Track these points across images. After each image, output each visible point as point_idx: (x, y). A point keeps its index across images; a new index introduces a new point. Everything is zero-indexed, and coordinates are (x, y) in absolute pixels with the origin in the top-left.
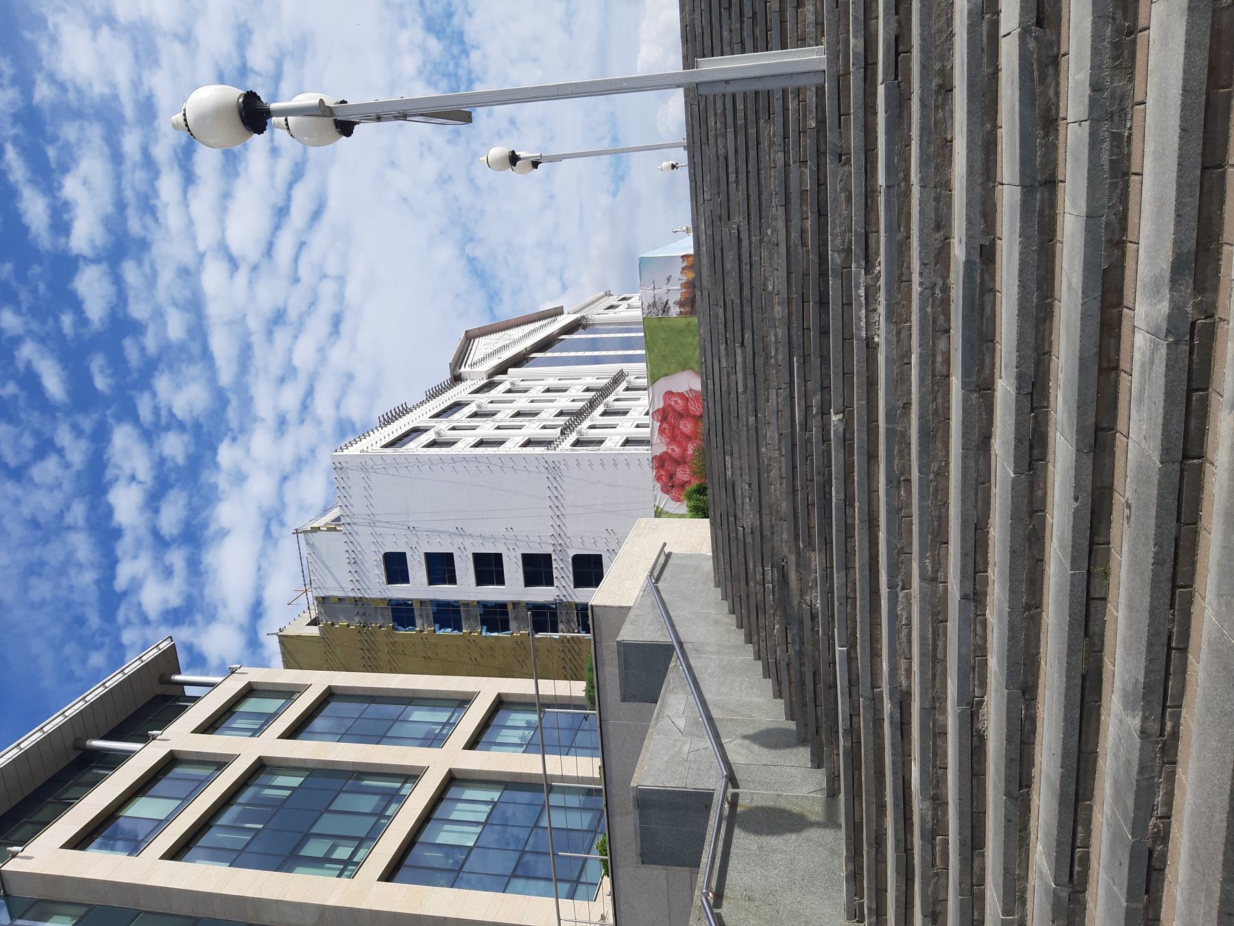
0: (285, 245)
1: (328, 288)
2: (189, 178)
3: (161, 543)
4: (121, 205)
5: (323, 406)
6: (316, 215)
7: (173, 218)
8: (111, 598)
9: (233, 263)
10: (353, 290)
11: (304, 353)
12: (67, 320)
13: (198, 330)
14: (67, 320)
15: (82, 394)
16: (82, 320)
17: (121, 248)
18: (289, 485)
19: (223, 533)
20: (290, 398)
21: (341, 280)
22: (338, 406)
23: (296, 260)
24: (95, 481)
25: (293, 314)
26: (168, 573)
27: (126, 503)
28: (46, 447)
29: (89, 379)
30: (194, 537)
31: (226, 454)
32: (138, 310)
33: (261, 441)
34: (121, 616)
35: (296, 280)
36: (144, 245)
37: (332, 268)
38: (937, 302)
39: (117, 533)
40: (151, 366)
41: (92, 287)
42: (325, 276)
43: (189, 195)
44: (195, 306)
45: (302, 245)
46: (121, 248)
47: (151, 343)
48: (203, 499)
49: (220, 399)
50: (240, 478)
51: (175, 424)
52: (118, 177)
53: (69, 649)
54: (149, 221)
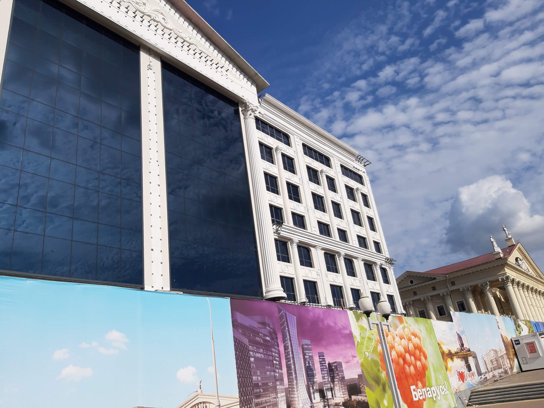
0: (510, 92)
1: (498, 114)
2: (532, 44)
3: (373, 92)
4: (511, 24)
5: (441, 130)
6: (532, 97)
7: (513, 44)
8: (349, 83)
9: (497, 74)
10: (499, 124)
11: (463, 115)
12: (457, 23)
13: (464, 70)
14: (457, 23)
15: (426, 42)
16: (457, 28)
17: (492, 30)
18: (404, 129)
19: (380, 111)
20: (441, 117)
21: (504, 117)
22: (443, 136)
23: (506, 97)
24: (394, 58)
25: (482, 105)
26: (362, 98)
27: (388, 72)
28: (404, 37)
29: (432, 43)
30: (378, 103)
31: (413, 101)
32: (467, 46)
33: (421, 112)
34: (344, 88)
35: (497, 100)
36: (496, 37)
37: (508, 112)
38: (189, 103)
39: (376, 76)
40: (444, 60)
41: (475, 25)
42: (503, 110)
43: (523, 47)
44: (475, 65)
45: (514, 98)
46: (492, 30)
47: (454, 56)
48: (394, 99)
49: (436, 90)
50: (404, 110)
51: (422, 76)
52: (525, 17)
53: (329, 76)
54: (508, 36)
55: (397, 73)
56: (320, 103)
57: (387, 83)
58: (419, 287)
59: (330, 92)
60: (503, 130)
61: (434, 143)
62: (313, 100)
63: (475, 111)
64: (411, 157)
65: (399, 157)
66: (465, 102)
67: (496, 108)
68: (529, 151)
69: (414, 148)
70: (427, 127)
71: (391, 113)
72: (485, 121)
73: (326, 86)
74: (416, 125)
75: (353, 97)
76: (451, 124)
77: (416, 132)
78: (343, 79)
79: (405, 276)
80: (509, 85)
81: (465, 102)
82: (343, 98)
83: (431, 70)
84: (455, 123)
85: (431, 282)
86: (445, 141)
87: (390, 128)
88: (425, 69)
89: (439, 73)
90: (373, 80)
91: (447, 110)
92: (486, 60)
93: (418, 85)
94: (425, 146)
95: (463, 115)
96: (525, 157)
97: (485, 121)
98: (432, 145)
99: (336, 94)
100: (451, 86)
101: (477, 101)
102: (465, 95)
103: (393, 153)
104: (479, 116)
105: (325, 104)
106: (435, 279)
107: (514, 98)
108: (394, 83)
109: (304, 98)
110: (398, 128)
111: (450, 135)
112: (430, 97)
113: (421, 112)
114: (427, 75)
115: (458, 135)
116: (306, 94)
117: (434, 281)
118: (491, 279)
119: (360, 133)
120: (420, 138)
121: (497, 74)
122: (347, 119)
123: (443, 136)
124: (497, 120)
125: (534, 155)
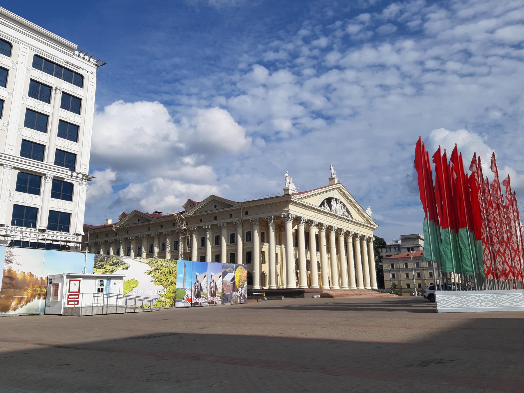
0: (501, 51)
5: (428, 77)
13: (464, 21)
18: (394, 70)
19: (375, 47)
20: (431, 64)
21: (489, 74)
22: (428, 83)
25: (472, 59)
30: (376, 40)
31: (408, 44)
34: (346, 19)
35: (487, 57)
37: (494, 70)
39: (380, 11)
44: (474, 18)
45: (503, 57)
48: (393, 38)
49: (433, 36)
50: (399, 51)
51: (424, 20)
55: (402, 12)
56: (320, 30)
57: (389, 21)
58: (204, 215)
59: (333, 20)
60: (487, 86)
61: (419, 88)
62: (315, 25)
63: (464, 63)
64: (394, 98)
65: (383, 96)
66: (456, 53)
67: (485, 64)
68: (501, 110)
69: (399, 90)
70: (416, 71)
71: (386, 52)
72: (471, 75)
73: (330, 13)
74: (405, 68)
75: (353, 29)
76: (438, 72)
77: (404, 76)
78: (348, 10)
79: (210, 200)
80: (501, 44)
81: (456, 53)
82: (344, 30)
83: (433, 16)
84: (444, 72)
85: (228, 209)
86: (429, 87)
87: (382, 67)
88: (426, 14)
89: (440, 19)
90: (377, 16)
91: (436, 58)
92: (485, 15)
93: (418, 29)
94: (409, 90)
95: (452, 65)
96: (496, 115)
97: (471, 75)
98: (417, 90)
99: (338, 23)
100: (448, 34)
101: (468, 54)
102: (458, 46)
103: (378, 91)
104: (467, 69)
105: (326, 33)
106: (232, 206)
107: (503, 57)
108: (393, 22)
109: (306, 22)
110: (388, 69)
111: (434, 83)
112: (425, 42)
113: (414, 56)
114: (428, 19)
115: (442, 84)
116: (310, 18)
117: (231, 209)
118: (277, 214)
119: (352, 67)
120: (408, 80)
121: (492, 31)
122: (342, 51)
123: (428, 83)
124: (482, 75)
125: (505, 114)
